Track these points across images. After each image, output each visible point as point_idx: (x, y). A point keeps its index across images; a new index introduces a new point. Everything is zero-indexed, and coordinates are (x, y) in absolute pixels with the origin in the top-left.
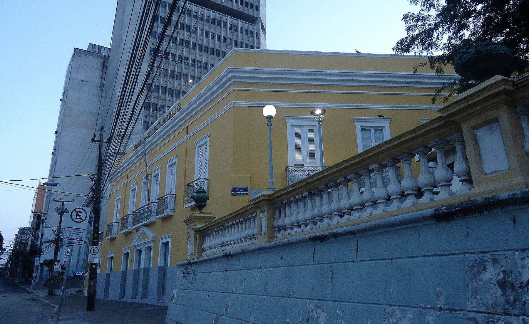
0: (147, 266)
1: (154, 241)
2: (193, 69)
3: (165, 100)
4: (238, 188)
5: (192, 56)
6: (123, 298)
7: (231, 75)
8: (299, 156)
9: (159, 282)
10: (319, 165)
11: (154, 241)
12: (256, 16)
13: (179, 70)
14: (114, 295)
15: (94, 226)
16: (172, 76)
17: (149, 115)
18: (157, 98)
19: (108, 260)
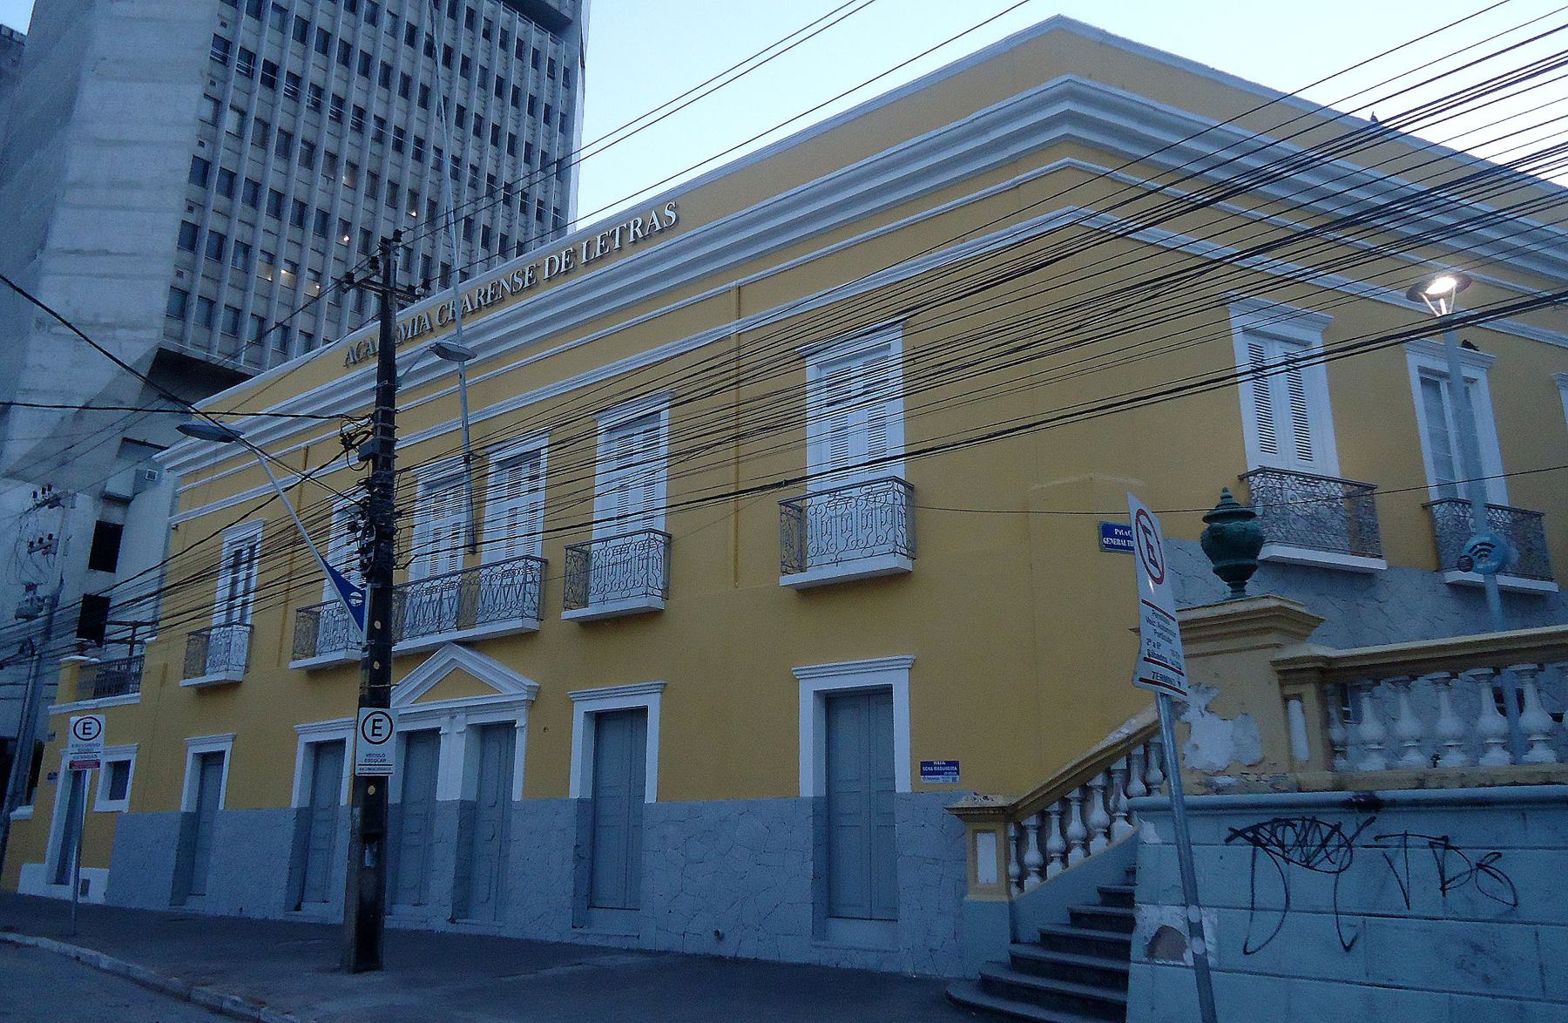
0: (472, 797)
1: (531, 705)
2: (357, 143)
3: (253, 226)
4: (1120, 528)
5: (355, 98)
6: (298, 908)
7: (1065, 130)
8: (1268, 446)
9: (578, 858)
10: (1335, 472)
11: (531, 705)
12: (567, 13)
13: (310, 136)
14: (535, 901)
15: (372, 633)
16: (285, 151)
17: (193, 270)
18: (227, 215)
19: (190, 768)
